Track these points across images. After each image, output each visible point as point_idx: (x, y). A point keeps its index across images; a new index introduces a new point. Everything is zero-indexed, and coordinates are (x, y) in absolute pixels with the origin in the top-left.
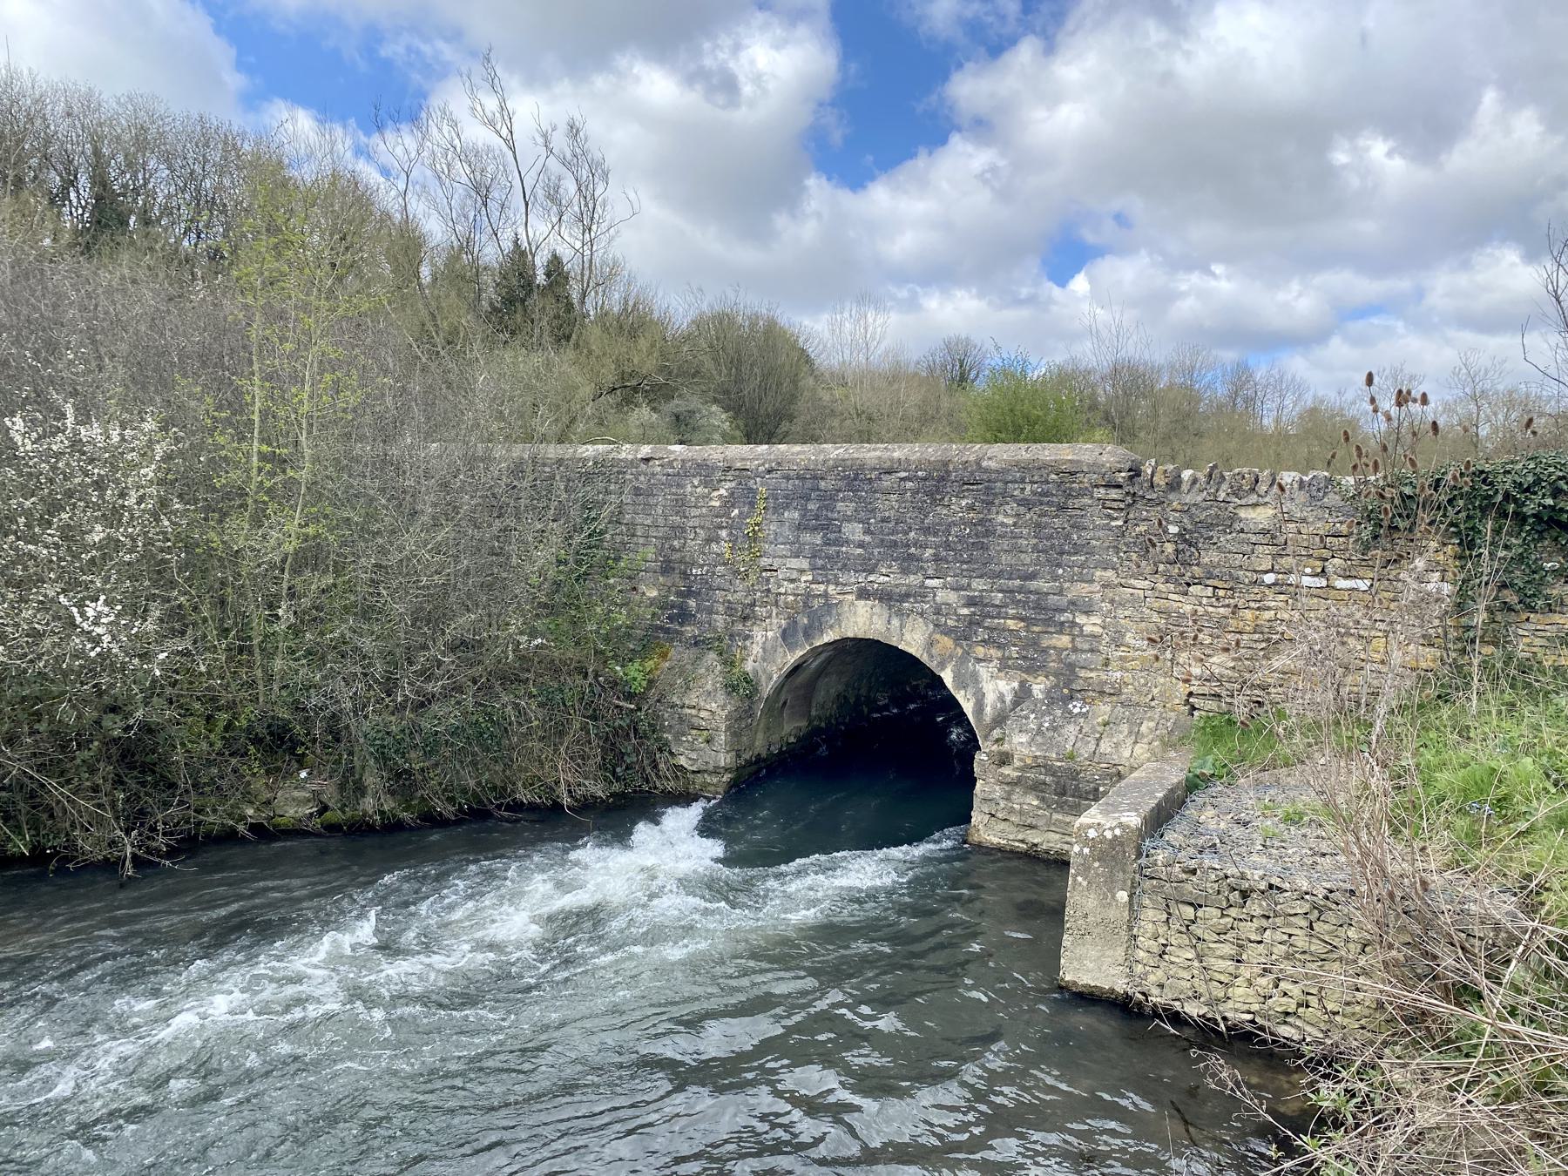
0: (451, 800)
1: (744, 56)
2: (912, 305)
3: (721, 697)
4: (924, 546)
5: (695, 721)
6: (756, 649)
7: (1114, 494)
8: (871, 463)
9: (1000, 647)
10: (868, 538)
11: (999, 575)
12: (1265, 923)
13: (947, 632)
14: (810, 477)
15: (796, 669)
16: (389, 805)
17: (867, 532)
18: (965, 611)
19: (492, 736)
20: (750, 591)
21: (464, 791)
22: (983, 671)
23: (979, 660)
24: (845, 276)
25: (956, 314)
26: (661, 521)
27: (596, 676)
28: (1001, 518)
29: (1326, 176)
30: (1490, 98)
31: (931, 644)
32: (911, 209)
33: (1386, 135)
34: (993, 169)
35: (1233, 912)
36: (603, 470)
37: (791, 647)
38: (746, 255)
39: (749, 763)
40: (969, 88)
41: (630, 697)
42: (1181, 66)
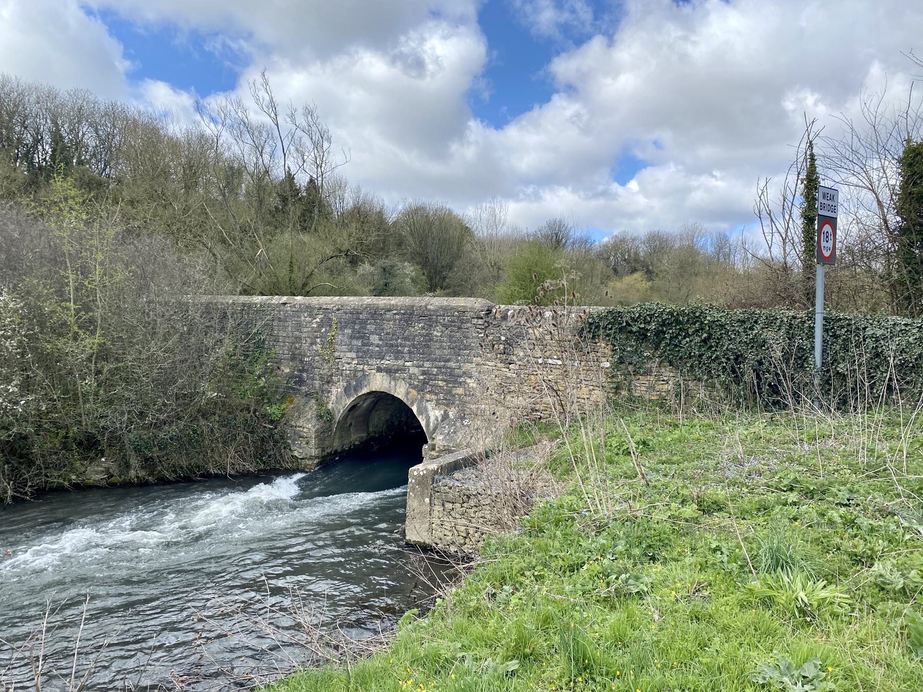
0: (175, 472)
1: (427, 46)
2: (537, 197)
3: (314, 421)
4: (404, 346)
5: (301, 434)
6: (333, 398)
7: (480, 322)
8: (381, 306)
9: (436, 394)
10: (381, 343)
11: (435, 360)
12: (476, 509)
13: (415, 387)
14: (356, 312)
15: (353, 408)
16: (142, 473)
17: (380, 339)
18: (422, 377)
19: (197, 441)
20: (330, 369)
21: (182, 468)
22: (430, 406)
23: (428, 401)
24: (491, 181)
25: (561, 204)
26: (290, 334)
27: (254, 413)
28: (435, 333)
29: (781, 117)
30: (876, 70)
31: (408, 393)
32: (533, 140)
33: (814, 90)
34: (578, 115)
35: (465, 505)
36: (262, 310)
37: (349, 396)
38: (434, 168)
39: (329, 454)
40: (564, 67)
41: (272, 422)
42: (690, 48)
